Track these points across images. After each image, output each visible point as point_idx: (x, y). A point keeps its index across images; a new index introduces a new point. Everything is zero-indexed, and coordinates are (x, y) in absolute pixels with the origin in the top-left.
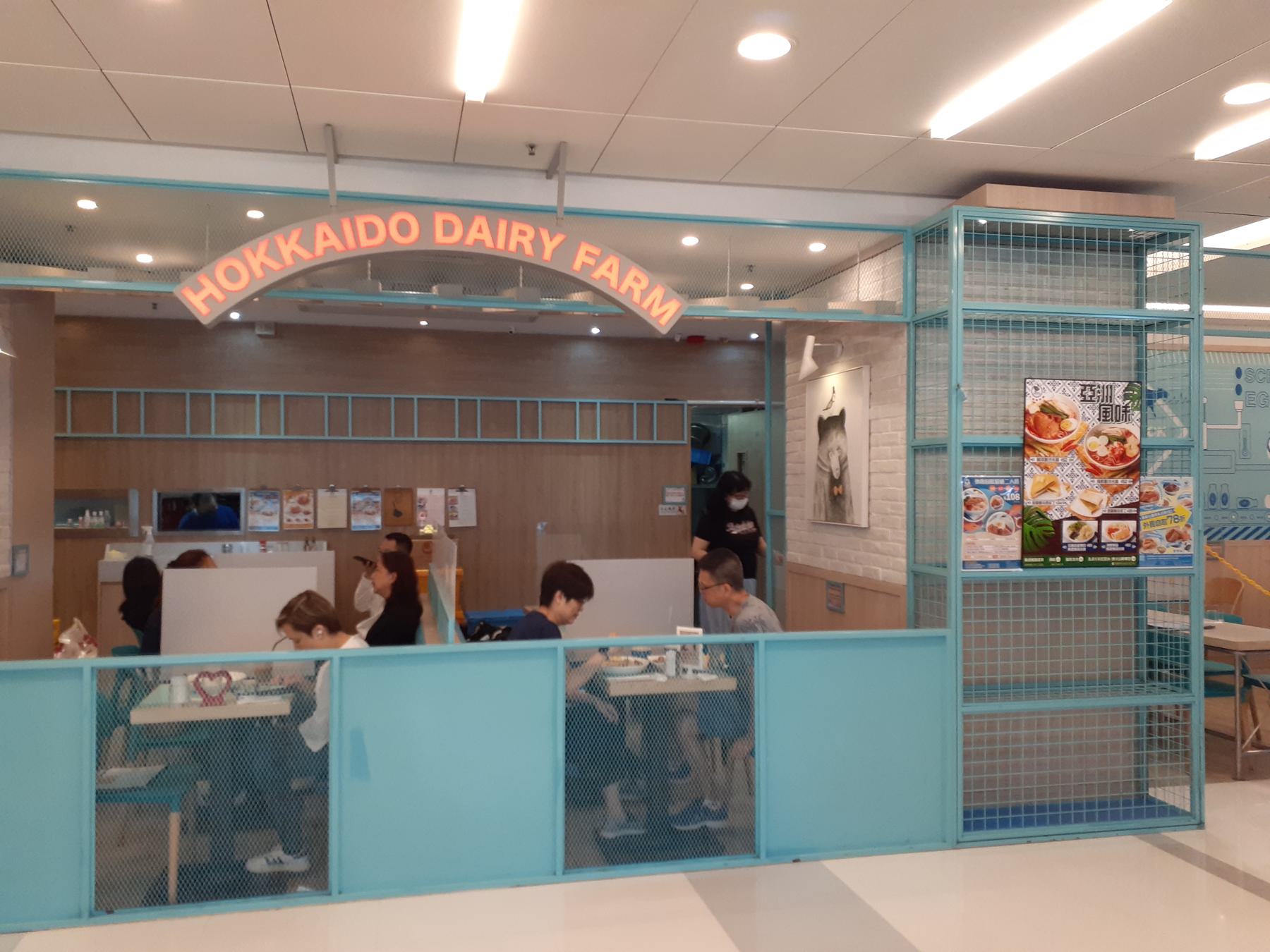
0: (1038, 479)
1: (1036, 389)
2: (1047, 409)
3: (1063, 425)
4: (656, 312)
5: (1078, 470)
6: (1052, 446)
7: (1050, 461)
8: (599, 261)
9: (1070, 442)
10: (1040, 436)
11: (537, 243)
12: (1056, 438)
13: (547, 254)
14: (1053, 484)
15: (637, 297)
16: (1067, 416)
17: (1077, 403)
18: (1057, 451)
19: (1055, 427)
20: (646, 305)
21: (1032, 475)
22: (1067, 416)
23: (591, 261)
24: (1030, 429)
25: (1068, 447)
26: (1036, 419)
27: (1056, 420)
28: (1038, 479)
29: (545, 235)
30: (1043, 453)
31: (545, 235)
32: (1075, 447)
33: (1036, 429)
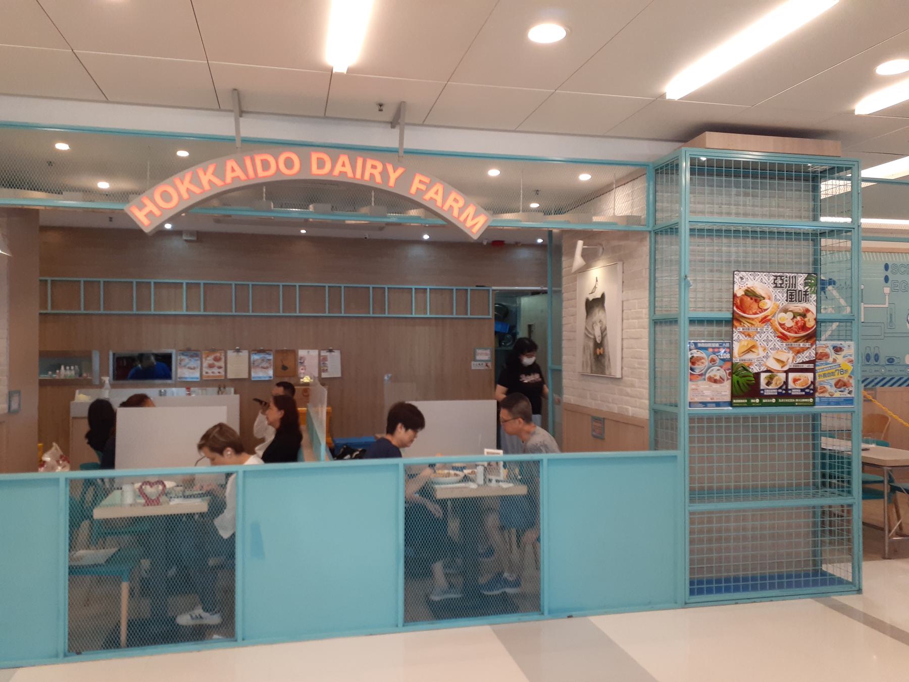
0: (743, 343)
1: (742, 278)
2: (750, 293)
3: (761, 304)
4: (469, 223)
5: (771, 336)
6: (753, 319)
7: (752, 330)
8: (429, 187)
9: (766, 317)
10: (744, 312)
11: (385, 174)
12: (756, 313)
13: (392, 182)
14: (753, 347)
15: (456, 213)
16: (764, 298)
17: (771, 289)
18: (757, 323)
19: (755, 306)
20: (462, 218)
21: (739, 341)
22: (764, 298)
23: (423, 187)
24: (737, 307)
25: (765, 320)
26: (742, 300)
27: (756, 301)
28: (743, 343)
29: (390, 168)
30: (747, 325)
31: (390, 168)
32: (769, 320)
33: (741, 307)
